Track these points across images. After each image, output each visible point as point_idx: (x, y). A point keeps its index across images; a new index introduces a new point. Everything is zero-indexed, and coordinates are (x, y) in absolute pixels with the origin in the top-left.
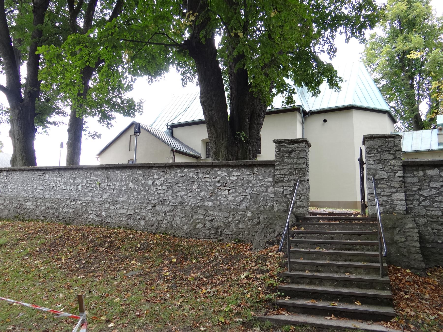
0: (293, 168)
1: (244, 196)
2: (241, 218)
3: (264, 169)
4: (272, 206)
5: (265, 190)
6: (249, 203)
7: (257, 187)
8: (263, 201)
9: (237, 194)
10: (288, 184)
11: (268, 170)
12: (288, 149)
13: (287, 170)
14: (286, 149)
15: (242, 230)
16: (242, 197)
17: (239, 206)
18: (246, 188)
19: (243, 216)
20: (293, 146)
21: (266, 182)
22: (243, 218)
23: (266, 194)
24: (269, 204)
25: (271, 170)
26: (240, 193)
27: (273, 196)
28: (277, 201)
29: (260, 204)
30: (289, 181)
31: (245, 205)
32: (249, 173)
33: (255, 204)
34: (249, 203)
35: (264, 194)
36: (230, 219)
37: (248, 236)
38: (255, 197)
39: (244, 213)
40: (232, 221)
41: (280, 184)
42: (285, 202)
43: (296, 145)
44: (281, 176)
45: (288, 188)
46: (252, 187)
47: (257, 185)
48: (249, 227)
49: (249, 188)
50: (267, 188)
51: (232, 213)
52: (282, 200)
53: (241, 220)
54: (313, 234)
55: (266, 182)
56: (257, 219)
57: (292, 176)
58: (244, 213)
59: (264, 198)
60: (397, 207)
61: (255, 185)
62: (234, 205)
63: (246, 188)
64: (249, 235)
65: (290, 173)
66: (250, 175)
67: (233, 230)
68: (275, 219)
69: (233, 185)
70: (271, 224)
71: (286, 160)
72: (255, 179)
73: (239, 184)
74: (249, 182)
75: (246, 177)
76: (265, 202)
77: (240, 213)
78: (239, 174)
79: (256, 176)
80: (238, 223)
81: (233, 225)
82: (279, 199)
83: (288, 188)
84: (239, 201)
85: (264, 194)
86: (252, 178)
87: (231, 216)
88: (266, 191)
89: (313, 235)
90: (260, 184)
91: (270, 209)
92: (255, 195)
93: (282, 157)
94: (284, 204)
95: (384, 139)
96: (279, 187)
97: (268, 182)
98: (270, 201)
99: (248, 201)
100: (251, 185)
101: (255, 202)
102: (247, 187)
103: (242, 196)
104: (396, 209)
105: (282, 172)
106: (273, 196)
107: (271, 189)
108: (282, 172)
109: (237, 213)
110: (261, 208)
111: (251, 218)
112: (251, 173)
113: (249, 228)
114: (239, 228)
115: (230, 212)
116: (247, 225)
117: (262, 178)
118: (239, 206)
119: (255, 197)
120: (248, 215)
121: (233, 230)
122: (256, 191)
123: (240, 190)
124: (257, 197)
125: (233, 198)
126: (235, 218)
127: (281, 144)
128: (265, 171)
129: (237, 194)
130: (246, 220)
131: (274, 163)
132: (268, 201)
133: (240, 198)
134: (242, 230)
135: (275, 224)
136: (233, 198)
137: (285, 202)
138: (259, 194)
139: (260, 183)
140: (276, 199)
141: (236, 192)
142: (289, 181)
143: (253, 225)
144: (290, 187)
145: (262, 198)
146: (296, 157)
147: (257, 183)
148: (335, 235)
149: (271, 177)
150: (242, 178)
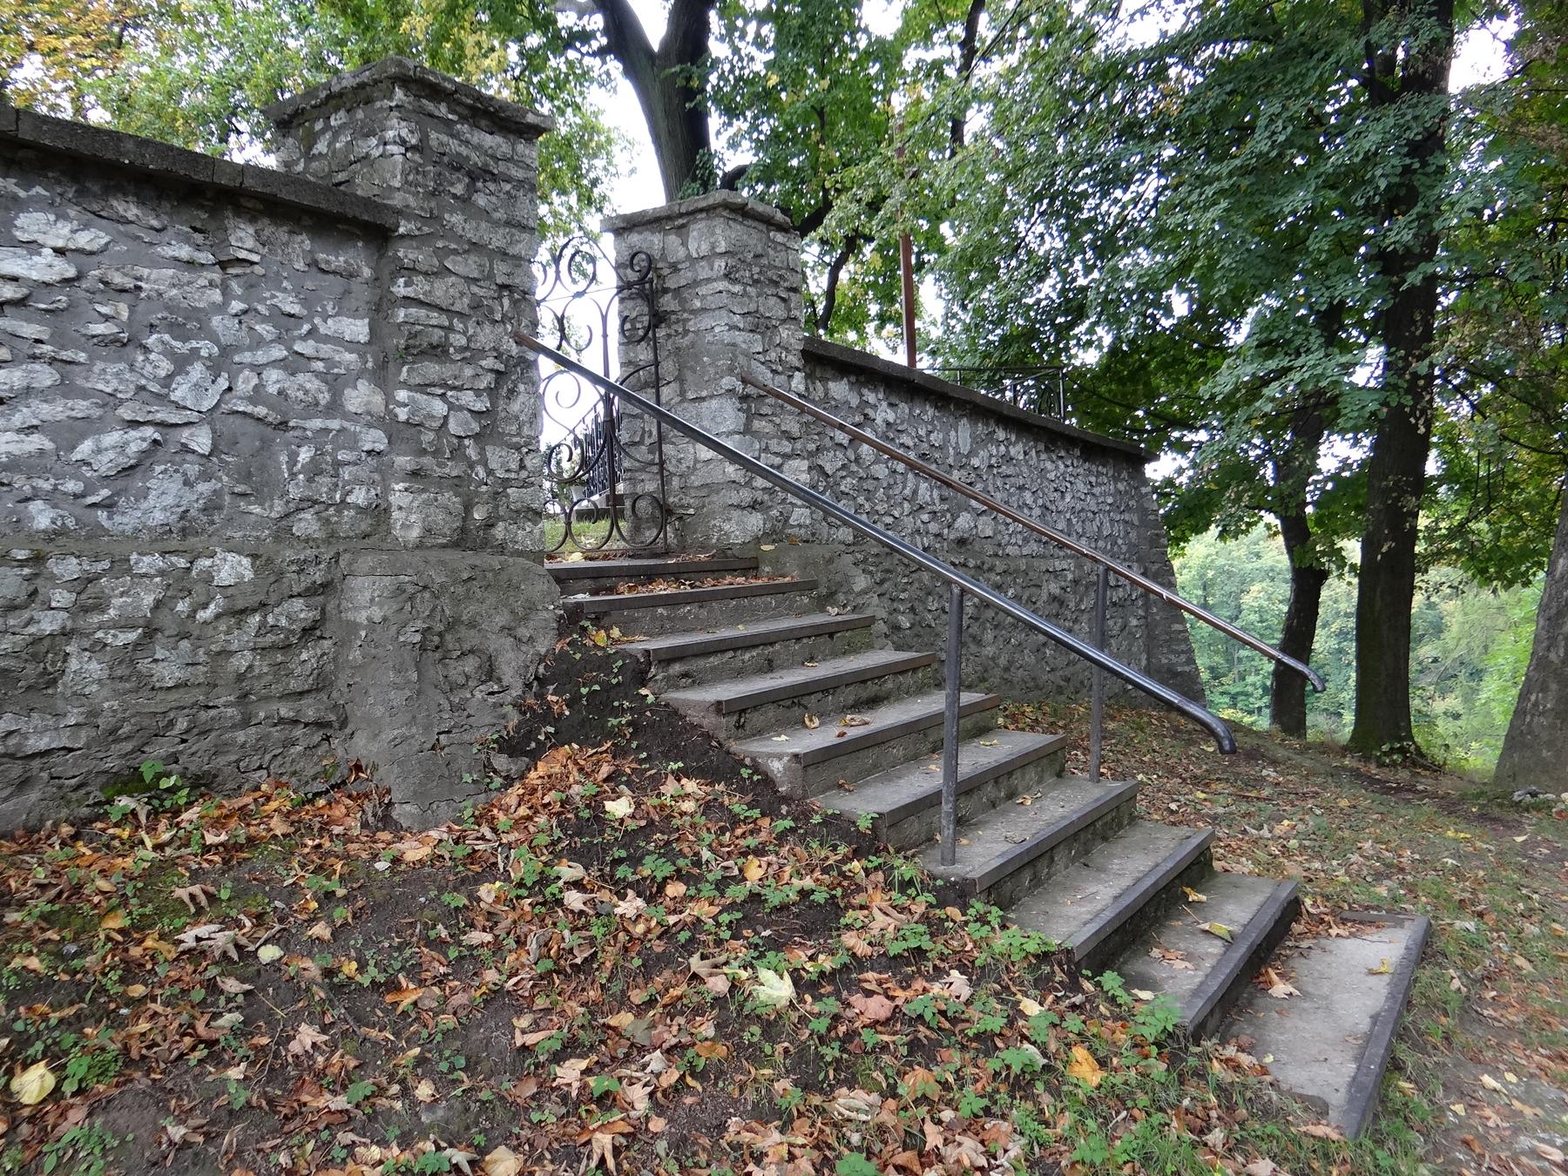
0: (490, 276)
1: (150, 432)
2: (158, 605)
3: (304, 242)
4: (379, 512)
5: (324, 398)
6: (204, 488)
7: (258, 369)
8: (314, 470)
9: (82, 407)
10: (468, 371)
11: (338, 260)
12: (464, 151)
13: (462, 286)
14: (454, 145)
15: (187, 698)
16: (138, 441)
17: (108, 505)
18: (165, 367)
19: (179, 584)
20: (489, 140)
21: (326, 339)
22: (182, 606)
23: (335, 424)
24: (359, 497)
25: (352, 258)
26: (111, 401)
27: (375, 439)
28: (415, 474)
29: (295, 492)
30: (471, 354)
31: (163, 496)
32: (185, 252)
33: (258, 494)
34: (204, 488)
35: (317, 423)
36: (49, 624)
37: (241, 736)
38: (252, 443)
39: (182, 563)
40: (66, 634)
41: (432, 370)
42: (458, 483)
43: (498, 139)
44: (436, 318)
45: (467, 398)
46: (215, 367)
47: (261, 357)
48: (241, 662)
49: (197, 371)
50: (336, 383)
51: (70, 568)
52: (439, 471)
53: (165, 619)
54: (715, 653)
55: (326, 339)
56: (298, 604)
57: (487, 328)
58: (182, 563)
59: (320, 453)
60: (794, 516)
61: (237, 349)
62: (52, 498)
63: (165, 367)
64: (245, 723)
65: (476, 306)
66: (190, 264)
67: (94, 713)
68: (461, 590)
69: (30, 330)
70: (452, 625)
71: (456, 219)
72: (236, 306)
73: (100, 329)
74: (186, 322)
75: (157, 279)
76: (324, 481)
77: (148, 563)
78: (84, 240)
79: (250, 287)
80: (137, 645)
81: (84, 668)
82: (427, 461)
83: (467, 398)
84: (105, 464)
85: (317, 423)
86: (216, 296)
87: (62, 597)
88: (334, 408)
89: (714, 660)
90: (278, 352)
91: (364, 526)
92: (250, 426)
93: (433, 194)
94: (450, 499)
95: (763, 227)
96: (422, 388)
97: (338, 340)
98: (363, 471)
99: (193, 469)
100: (206, 348)
101: (256, 481)
102: (181, 363)
103: (134, 424)
104: (791, 522)
105: (441, 290)
106: (375, 439)
107: (362, 396)
108: (441, 290)
109: (121, 566)
110: (306, 524)
111: (253, 601)
112: (205, 257)
113: (240, 678)
114: (145, 684)
115: (38, 559)
116: (226, 653)
117: (295, 309)
118: (108, 505)
119: (248, 444)
120: (225, 576)
121: (94, 713)
122: (257, 395)
123: (108, 377)
124: (266, 445)
125: (36, 442)
126: (100, 606)
127: (429, 106)
128: (313, 264)
129: (82, 407)
130: (203, 615)
131: (389, 221)
132: (346, 473)
133: (112, 438)
134: (187, 698)
135: (472, 625)
136: (36, 442)
137: (458, 483)
138: (283, 425)
139: (278, 339)
140: (404, 461)
141: (65, 389)
142: (471, 354)
143: (274, 647)
144: (478, 393)
145: (305, 455)
146: (500, 215)
147: (259, 343)
148: (777, 647)
149: (355, 314)
150: (118, 279)
